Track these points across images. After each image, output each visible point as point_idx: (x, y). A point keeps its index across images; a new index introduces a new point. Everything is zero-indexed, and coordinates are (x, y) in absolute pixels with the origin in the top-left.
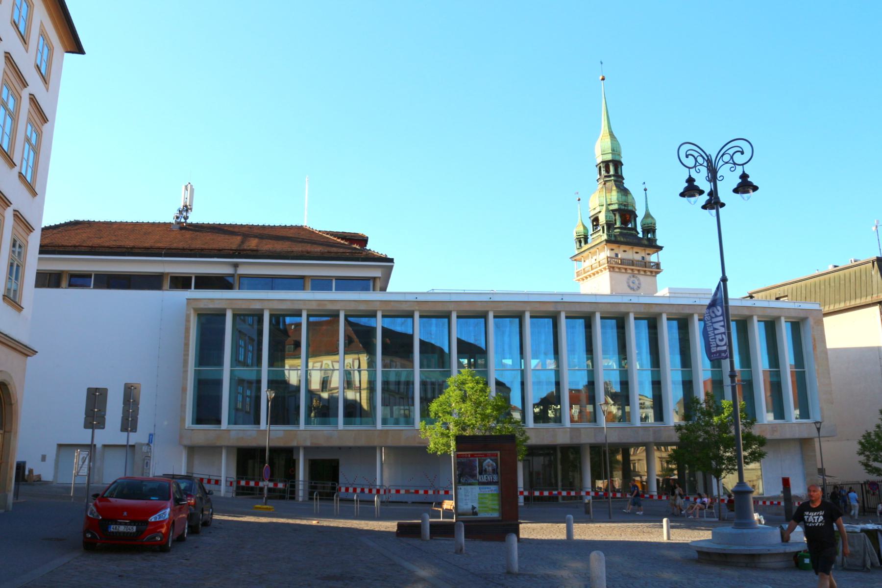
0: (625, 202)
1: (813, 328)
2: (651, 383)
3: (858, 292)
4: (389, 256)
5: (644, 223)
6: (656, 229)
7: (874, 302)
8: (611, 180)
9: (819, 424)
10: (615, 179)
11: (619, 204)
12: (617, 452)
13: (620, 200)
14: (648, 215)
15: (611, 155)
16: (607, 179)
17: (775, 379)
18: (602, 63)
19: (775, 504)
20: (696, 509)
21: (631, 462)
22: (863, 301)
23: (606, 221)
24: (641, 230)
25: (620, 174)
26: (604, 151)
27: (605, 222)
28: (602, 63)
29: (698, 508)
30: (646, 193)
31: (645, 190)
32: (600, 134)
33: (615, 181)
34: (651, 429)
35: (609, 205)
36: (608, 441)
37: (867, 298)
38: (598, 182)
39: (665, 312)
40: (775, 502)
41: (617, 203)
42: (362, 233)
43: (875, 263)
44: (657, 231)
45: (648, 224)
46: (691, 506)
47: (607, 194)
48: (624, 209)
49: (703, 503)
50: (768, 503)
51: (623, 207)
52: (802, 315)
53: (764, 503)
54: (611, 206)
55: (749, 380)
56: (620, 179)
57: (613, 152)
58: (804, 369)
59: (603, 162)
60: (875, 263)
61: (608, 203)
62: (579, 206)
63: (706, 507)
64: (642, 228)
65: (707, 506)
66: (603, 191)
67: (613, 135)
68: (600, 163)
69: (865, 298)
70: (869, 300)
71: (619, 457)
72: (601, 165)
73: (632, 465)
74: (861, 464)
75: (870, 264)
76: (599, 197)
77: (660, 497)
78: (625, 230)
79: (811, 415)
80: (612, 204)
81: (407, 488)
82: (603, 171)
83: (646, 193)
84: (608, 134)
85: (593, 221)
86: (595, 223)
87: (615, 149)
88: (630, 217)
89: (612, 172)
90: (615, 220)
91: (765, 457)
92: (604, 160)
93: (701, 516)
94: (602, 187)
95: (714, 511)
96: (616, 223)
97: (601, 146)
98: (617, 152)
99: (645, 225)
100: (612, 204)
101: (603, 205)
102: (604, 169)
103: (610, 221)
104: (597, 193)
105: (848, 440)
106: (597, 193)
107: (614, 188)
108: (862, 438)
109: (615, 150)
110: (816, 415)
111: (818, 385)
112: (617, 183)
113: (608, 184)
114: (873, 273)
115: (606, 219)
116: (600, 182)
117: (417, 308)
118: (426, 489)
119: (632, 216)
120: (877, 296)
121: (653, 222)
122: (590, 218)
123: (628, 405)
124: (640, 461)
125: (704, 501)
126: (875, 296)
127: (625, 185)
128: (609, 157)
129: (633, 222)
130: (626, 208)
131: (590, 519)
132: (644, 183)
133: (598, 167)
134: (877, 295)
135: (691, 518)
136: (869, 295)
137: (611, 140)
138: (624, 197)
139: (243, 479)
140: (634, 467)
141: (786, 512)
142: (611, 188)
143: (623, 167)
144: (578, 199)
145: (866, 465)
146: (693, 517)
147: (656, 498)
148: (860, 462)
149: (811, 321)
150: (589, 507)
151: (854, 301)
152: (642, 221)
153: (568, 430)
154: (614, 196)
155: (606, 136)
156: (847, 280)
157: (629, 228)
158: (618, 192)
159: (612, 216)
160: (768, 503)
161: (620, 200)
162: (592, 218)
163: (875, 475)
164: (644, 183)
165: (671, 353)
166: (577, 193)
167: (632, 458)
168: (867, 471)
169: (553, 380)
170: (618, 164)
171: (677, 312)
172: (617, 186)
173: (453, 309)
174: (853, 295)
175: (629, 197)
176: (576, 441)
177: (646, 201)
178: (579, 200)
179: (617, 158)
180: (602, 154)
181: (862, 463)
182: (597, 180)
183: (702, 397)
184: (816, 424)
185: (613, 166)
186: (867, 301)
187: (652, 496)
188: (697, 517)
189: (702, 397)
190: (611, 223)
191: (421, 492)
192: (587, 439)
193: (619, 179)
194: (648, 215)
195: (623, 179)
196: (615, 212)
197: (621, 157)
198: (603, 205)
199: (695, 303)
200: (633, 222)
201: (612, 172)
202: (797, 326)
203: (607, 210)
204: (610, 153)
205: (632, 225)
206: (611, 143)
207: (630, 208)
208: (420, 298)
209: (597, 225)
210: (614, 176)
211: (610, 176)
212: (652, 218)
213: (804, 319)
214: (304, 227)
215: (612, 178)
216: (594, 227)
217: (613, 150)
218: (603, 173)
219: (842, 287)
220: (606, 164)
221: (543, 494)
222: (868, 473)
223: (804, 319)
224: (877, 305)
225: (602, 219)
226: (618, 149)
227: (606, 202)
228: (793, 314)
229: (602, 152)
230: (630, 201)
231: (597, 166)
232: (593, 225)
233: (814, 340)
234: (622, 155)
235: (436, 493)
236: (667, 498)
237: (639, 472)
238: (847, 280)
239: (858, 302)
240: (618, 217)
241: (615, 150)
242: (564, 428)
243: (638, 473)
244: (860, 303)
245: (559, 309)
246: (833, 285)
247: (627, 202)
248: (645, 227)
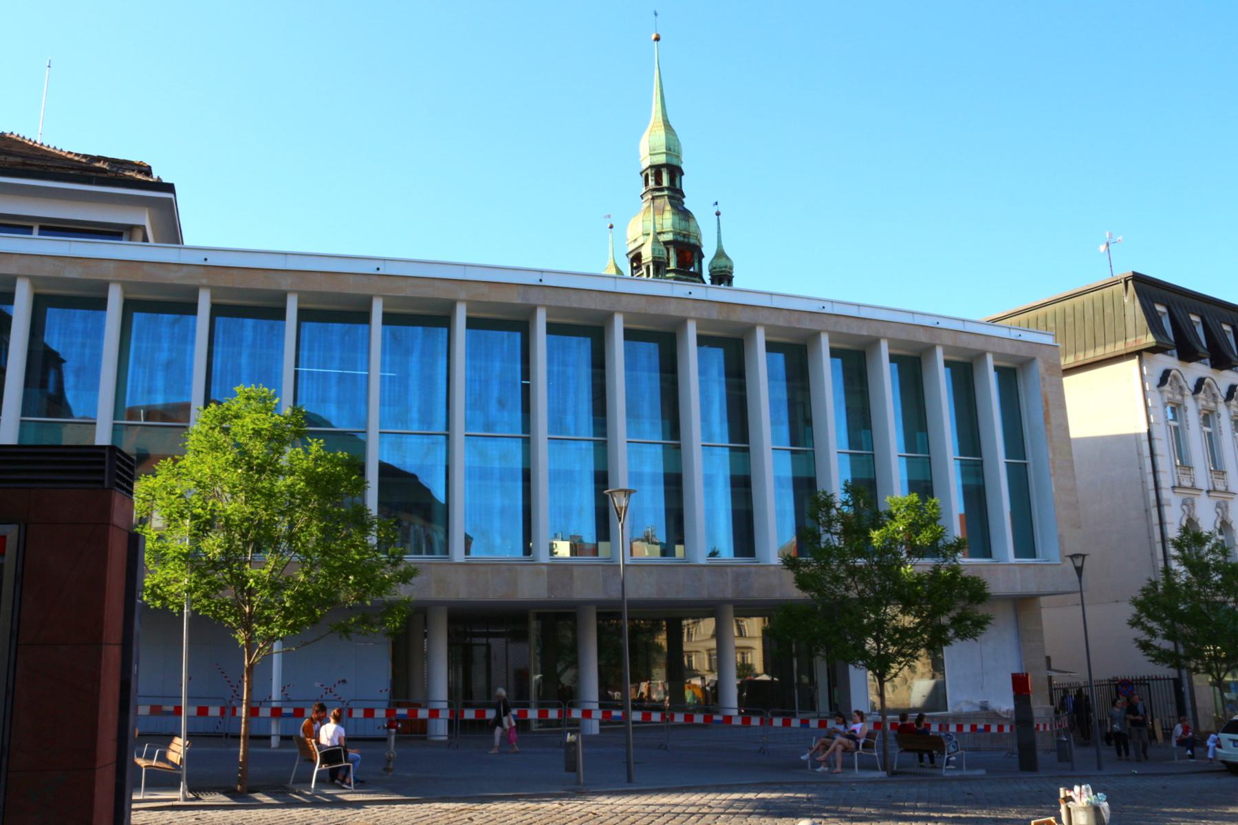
0: (685, 230)
1: (1044, 379)
2: (729, 484)
3: (1100, 335)
4: (165, 180)
5: (714, 266)
6: (733, 277)
7: (1129, 351)
8: (663, 196)
9: (1080, 559)
10: (670, 194)
11: (675, 234)
12: (655, 629)
13: (677, 226)
14: (720, 254)
15: (665, 155)
16: (658, 194)
17: (972, 481)
18: (656, 14)
19: (981, 730)
20: (835, 750)
21: (685, 654)
22: (1110, 350)
23: (654, 258)
24: (709, 277)
25: (678, 186)
26: (654, 150)
27: (650, 259)
28: (656, 14)
29: (840, 748)
30: (718, 220)
31: (718, 214)
32: (648, 123)
33: (669, 197)
34: (729, 570)
35: (660, 233)
36: (632, 594)
37: (1117, 345)
38: (642, 198)
39: (762, 325)
40: (981, 727)
41: (671, 231)
42: (139, 161)
43: (1130, 283)
44: (734, 279)
45: (721, 268)
46: (823, 744)
47: (657, 217)
48: (683, 241)
49: (852, 736)
50: (967, 729)
51: (681, 239)
52: (1024, 352)
53: (960, 728)
54: (662, 235)
55: (925, 481)
56: (678, 196)
57: (669, 152)
58: (1025, 459)
59: (651, 167)
60: (1130, 283)
61: (658, 231)
62: (610, 235)
63: (858, 744)
64: (710, 275)
65: (862, 741)
66: (649, 211)
67: (670, 126)
68: (647, 169)
69: (1113, 345)
70: (1120, 348)
71: (662, 639)
72: (649, 171)
73: (686, 659)
74: (1137, 644)
75: (1120, 284)
76: (643, 221)
77: (746, 721)
78: (684, 275)
79: (1039, 550)
80: (663, 233)
81: (157, 702)
82: (652, 180)
83: (718, 220)
84: (662, 124)
85: (633, 260)
86: (635, 265)
87: (672, 147)
88: (692, 254)
89: (665, 183)
90: (668, 259)
91: (987, 626)
92: (653, 164)
93: (848, 766)
94: (649, 207)
95: (876, 754)
96: (668, 264)
97: (649, 142)
98: (674, 151)
99: (715, 268)
100: (663, 233)
101: (648, 234)
102: (653, 178)
103: (660, 258)
104: (640, 217)
105: (1117, 601)
106: (640, 217)
107: (668, 207)
108: (1140, 593)
109: (672, 149)
110: (1051, 549)
111: (1054, 489)
112: (673, 201)
113: (658, 201)
114: (1126, 301)
115: (653, 254)
116: (645, 198)
117: (204, 281)
118: (369, 705)
119: (696, 255)
120: (1136, 341)
121: (728, 264)
122: (627, 255)
123: (681, 542)
124: (697, 654)
125: (854, 731)
126: (1130, 340)
127: (685, 206)
128: (662, 159)
129: (696, 265)
130: (686, 240)
131: (578, 783)
132: (716, 203)
133: (644, 175)
134: (1134, 339)
135: (824, 772)
136: (1120, 340)
137: (666, 133)
138: (683, 223)
139: (756, 713)
140: (690, 662)
141: (1019, 748)
142: (664, 208)
143: (683, 177)
144: (609, 225)
145: (1145, 646)
146: (827, 769)
147: (737, 721)
148: (1136, 640)
149: (1040, 366)
150: (576, 753)
151: (1092, 352)
152: (711, 263)
153: (545, 568)
154: (668, 220)
155: (657, 127)
156: (1078, 316)
157: (691, 272)
158: (673, 214)
159: (662, 250)
160: (967, 729)
161: (677, 226)
162: (631, 256)
163: (1167, 665)
164: (716, 203)
165: (775, 422)
166: (609, 216)
167: (685, 649)
168: (1149, 658)
169: (518, 464)
170: (675, 171)
171: (786, 325)
172: (672, 205)
173: (289, 288)
174: (1089, 341)
175: (692, 224)
176: (561, 595)
177: (719, 232)
178: (611, 227)
179: (674, 162)
180: (651, 155)
181: (1140, 642)
182: (641, 196)
183: (839, 495)
184: (1074, 559)
185: (667, 173)
186: (1116, 349)
187: (728, 719)
188: (839, 769)
189: (839, 495)
190: (661, 260)
191: (214, 711)
192: (584, 590)
193: (676, 196)
194: (720, 254)
195: (684, 197)
196: (669, 246)
197: (682, 163)
198: (648, 234)
199: (824, 311)
200: (696, 265)
201: (665, 183)
202: (1010, 376)
203: (656, 241)
204: (663, 153)
205: (694, 269)
206: (666, 138)
207: (693, 241)
208: (214, 260)
209: (638, 268)
210: (668, 188)
211: (662, 190)
212: (728, 258)
213: (1027, 362)
214: (8, 135)
215: (666, 193)
216: (634, 271)
217: (668, 149)
218: (652, 184)
219: (1069, 328)
220: (657, 169)
221: (546, 715)
222: (1153, 661)
223: (1027, 362)
224: (1135, 358)
225: (647, 255)
226: (676, 148)
227: (654, 227)
228: (1009, 350)
229: (650, 151)
230: (692, 229)
231: (641, 174)
232: (633, 268)
233: (1046, 402)
234: (683, 159)
235: (228, 712)
236: (762, 722)
237: (697, 670)
238: (1078, 316)
239: (1100, 353)
240: (672, 253)
241: (672, 149)
242: (536, 564)
243: (696, 672)
244: (1104, 355)
245: (533, 301)
246: (1053, 325)
247: (688, 231)
248: (715, 272)
